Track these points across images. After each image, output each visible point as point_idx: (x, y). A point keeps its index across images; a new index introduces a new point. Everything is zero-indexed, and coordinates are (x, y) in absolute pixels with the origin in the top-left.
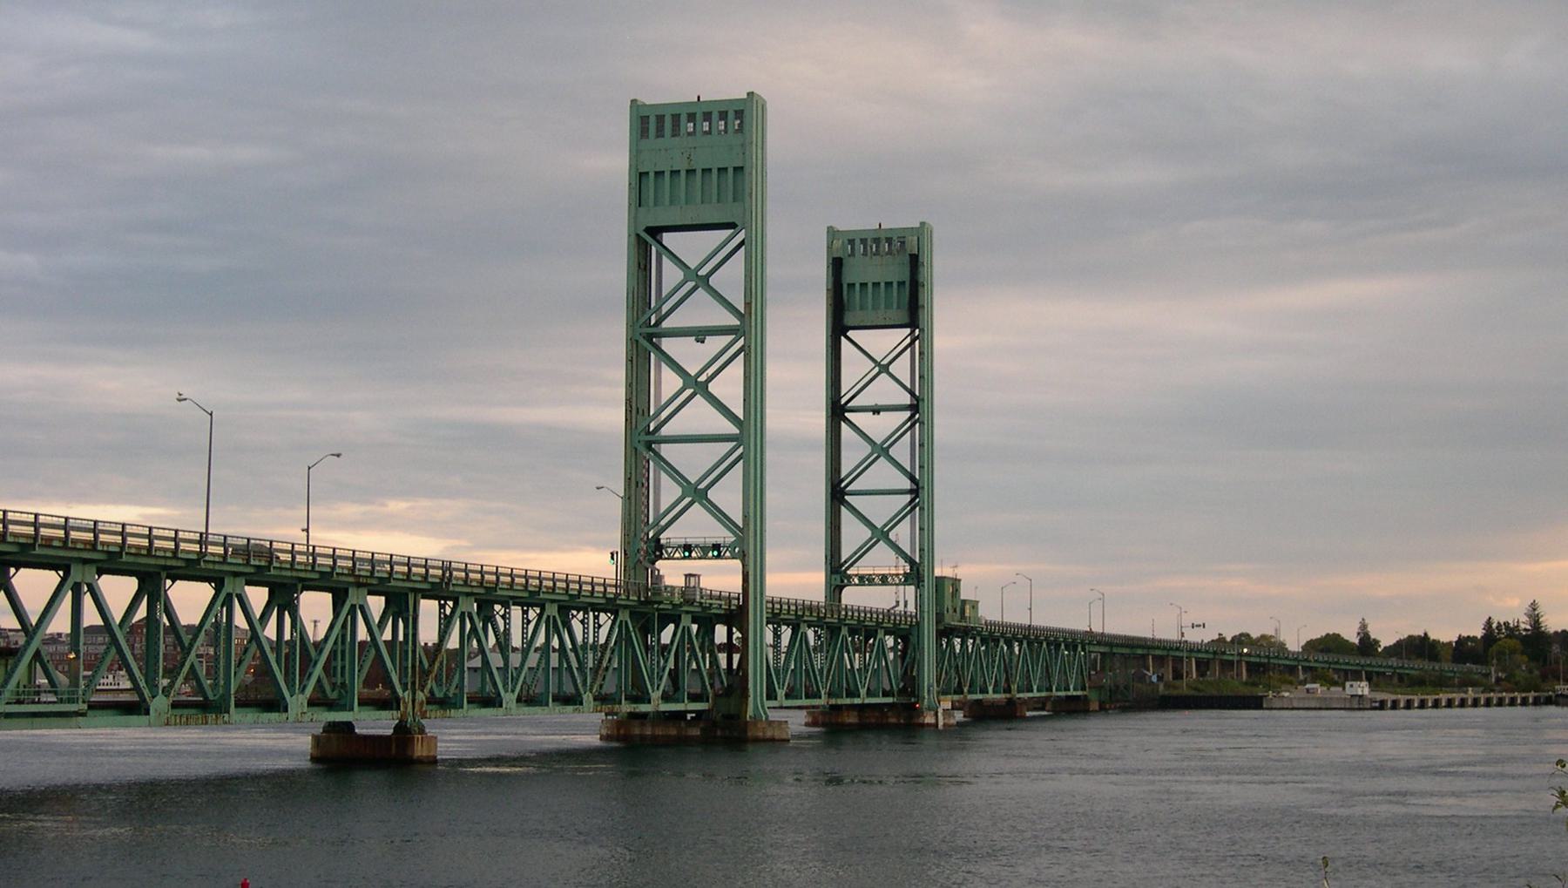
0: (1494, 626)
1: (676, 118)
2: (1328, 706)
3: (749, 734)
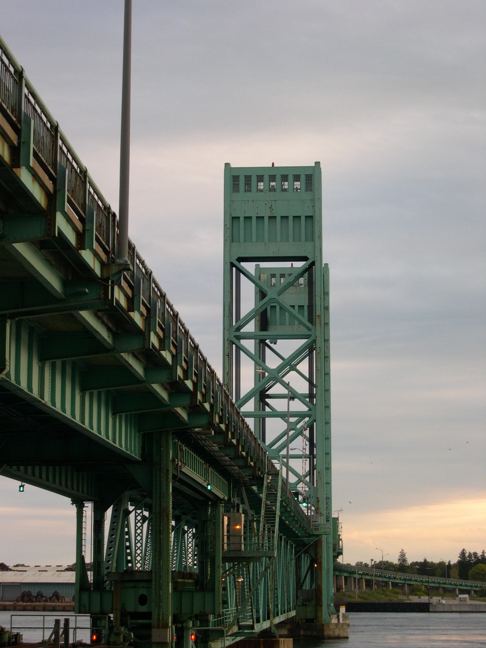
0: (467, 555)
1: (248, 178)
2: (478, 610)
3: (325, 633)
